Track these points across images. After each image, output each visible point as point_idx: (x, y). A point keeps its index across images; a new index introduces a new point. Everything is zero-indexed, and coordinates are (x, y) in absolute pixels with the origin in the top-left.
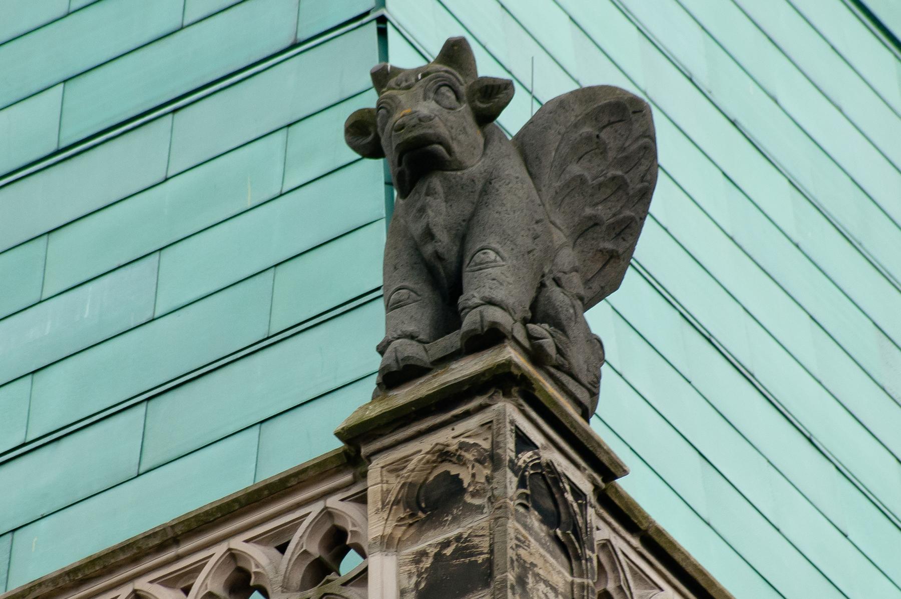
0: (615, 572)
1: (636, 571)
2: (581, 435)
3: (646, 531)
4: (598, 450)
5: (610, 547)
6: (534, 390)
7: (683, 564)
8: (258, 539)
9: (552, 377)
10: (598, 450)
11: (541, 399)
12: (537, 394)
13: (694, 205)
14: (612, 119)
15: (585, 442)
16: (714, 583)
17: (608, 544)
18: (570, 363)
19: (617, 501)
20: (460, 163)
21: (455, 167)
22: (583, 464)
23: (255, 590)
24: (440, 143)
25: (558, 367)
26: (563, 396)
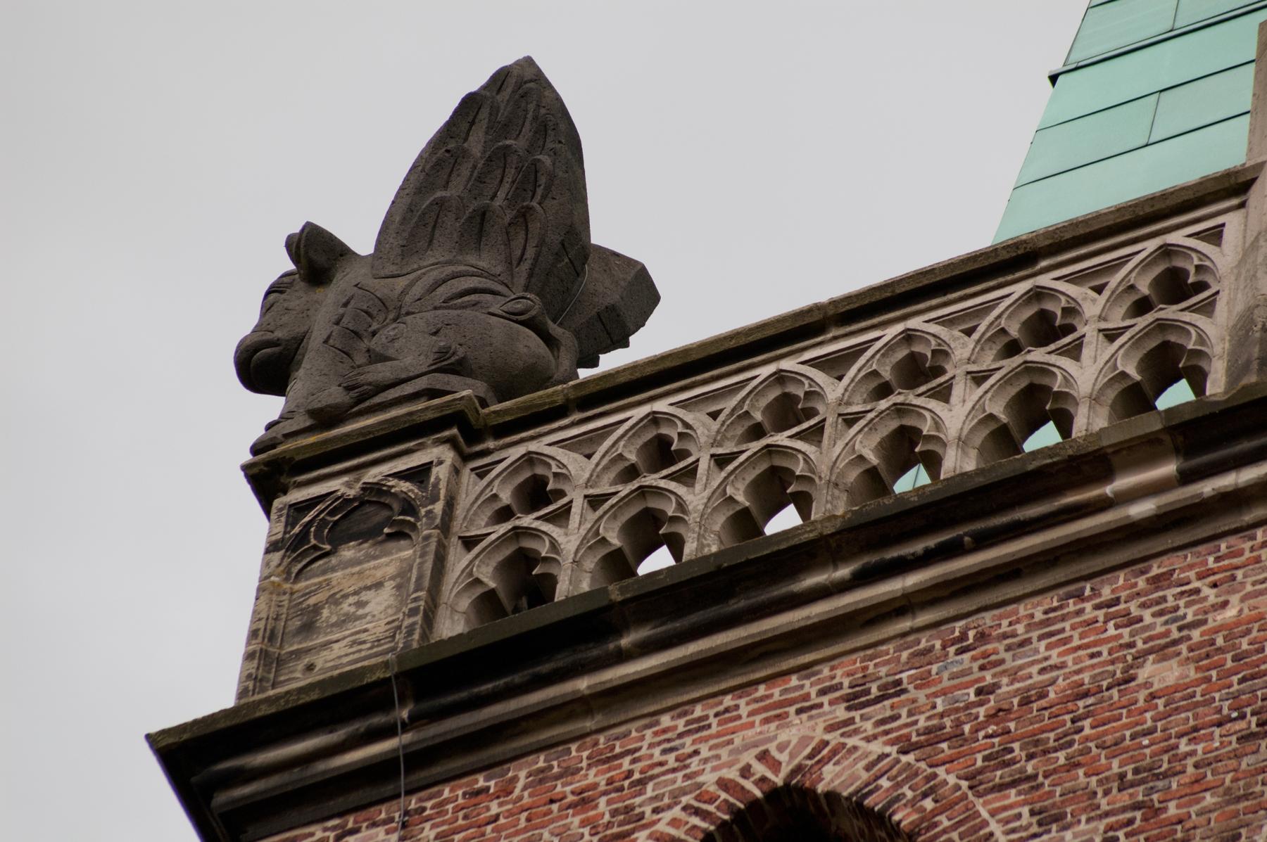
0: (277, 556)
1: (588, 438)
2: (382, 429)
3: (568, 400)
4: (414, 417)
5: (535, 456)
6: (291, 459)
7: (638, 375)
8: (1197, 306)
9: (361, 414)
10: (414, 417)
11: (307, 455)
12: (298, 458)
13: (1143, 99)
14: (470, 119)
15: (392, 429)
16: (686, 350)
17: (909, 332)
18: (370, 384)
19: (508, 418)
20: (294, 338)
21: (296, 346)
22: (411, 444)
23: (919, 462)
24: (256, 351)
25: (360, 400)
26: (389, 412)
